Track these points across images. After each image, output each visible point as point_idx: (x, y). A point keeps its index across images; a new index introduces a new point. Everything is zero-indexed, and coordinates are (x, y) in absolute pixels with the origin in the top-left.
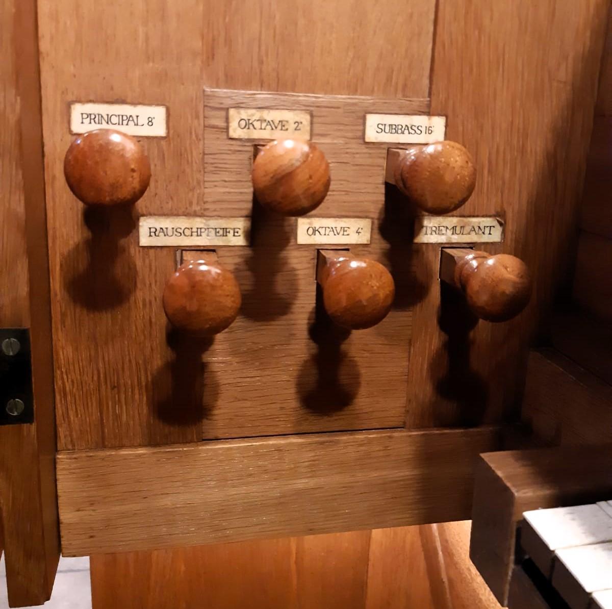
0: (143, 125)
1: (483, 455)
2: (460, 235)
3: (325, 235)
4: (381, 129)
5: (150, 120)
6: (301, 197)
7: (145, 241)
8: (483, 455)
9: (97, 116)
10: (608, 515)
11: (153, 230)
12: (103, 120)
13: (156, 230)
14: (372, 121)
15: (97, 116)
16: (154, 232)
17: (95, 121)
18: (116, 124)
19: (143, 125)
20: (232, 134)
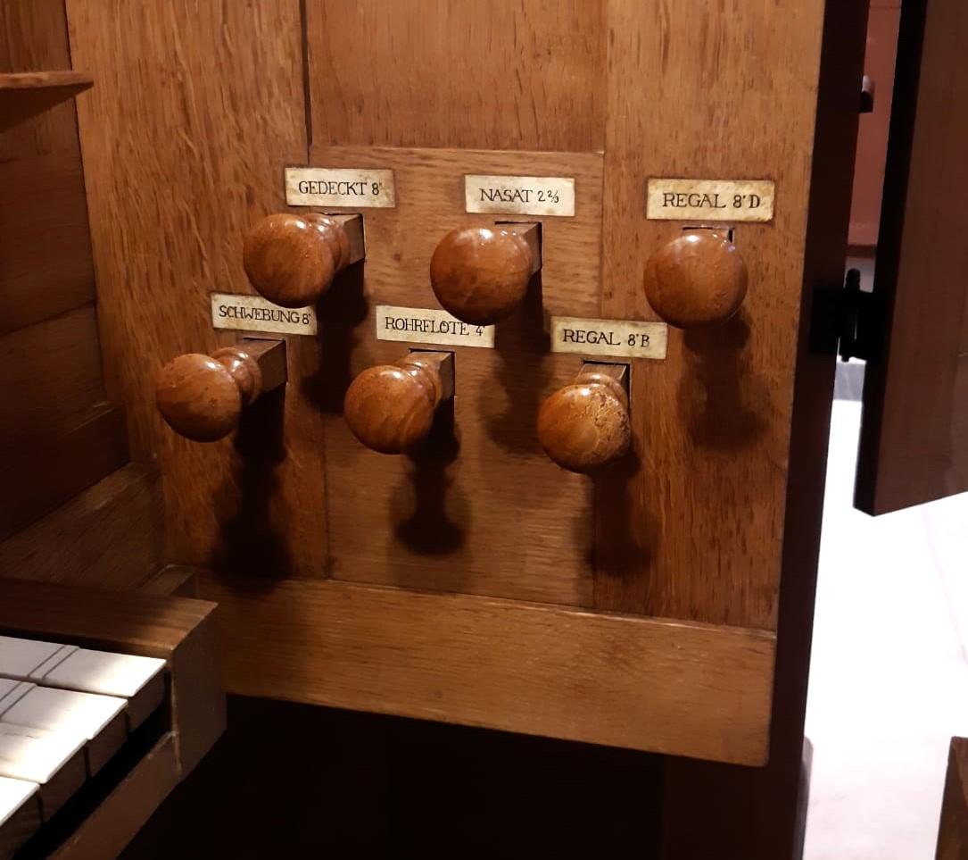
0: (724, 206)
1: (215, 605)
2: (279, 322)
3: (433, 331)
4: (668, 199)
5: (375, 186)
6: (479, 281)
7: (383, 333)
8: (215, 605)
9: (676, 197)
10: (33, 672)
11: (569, 333)
12: (484, 195)
13: (573, 333)
14: (474, 185)
15: (676, 197)
16: (392, 323)
17: (672, 203)
18: (686, 205)
19: (724, 206)
20: (768, 216)
